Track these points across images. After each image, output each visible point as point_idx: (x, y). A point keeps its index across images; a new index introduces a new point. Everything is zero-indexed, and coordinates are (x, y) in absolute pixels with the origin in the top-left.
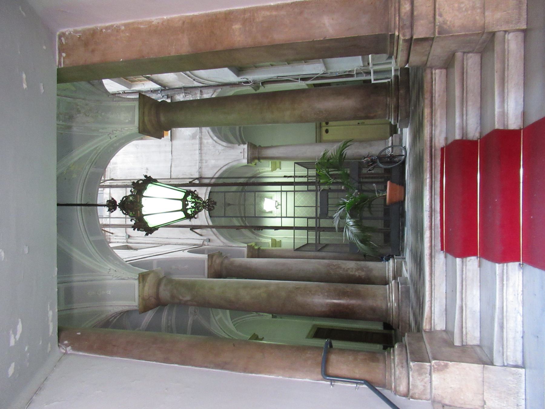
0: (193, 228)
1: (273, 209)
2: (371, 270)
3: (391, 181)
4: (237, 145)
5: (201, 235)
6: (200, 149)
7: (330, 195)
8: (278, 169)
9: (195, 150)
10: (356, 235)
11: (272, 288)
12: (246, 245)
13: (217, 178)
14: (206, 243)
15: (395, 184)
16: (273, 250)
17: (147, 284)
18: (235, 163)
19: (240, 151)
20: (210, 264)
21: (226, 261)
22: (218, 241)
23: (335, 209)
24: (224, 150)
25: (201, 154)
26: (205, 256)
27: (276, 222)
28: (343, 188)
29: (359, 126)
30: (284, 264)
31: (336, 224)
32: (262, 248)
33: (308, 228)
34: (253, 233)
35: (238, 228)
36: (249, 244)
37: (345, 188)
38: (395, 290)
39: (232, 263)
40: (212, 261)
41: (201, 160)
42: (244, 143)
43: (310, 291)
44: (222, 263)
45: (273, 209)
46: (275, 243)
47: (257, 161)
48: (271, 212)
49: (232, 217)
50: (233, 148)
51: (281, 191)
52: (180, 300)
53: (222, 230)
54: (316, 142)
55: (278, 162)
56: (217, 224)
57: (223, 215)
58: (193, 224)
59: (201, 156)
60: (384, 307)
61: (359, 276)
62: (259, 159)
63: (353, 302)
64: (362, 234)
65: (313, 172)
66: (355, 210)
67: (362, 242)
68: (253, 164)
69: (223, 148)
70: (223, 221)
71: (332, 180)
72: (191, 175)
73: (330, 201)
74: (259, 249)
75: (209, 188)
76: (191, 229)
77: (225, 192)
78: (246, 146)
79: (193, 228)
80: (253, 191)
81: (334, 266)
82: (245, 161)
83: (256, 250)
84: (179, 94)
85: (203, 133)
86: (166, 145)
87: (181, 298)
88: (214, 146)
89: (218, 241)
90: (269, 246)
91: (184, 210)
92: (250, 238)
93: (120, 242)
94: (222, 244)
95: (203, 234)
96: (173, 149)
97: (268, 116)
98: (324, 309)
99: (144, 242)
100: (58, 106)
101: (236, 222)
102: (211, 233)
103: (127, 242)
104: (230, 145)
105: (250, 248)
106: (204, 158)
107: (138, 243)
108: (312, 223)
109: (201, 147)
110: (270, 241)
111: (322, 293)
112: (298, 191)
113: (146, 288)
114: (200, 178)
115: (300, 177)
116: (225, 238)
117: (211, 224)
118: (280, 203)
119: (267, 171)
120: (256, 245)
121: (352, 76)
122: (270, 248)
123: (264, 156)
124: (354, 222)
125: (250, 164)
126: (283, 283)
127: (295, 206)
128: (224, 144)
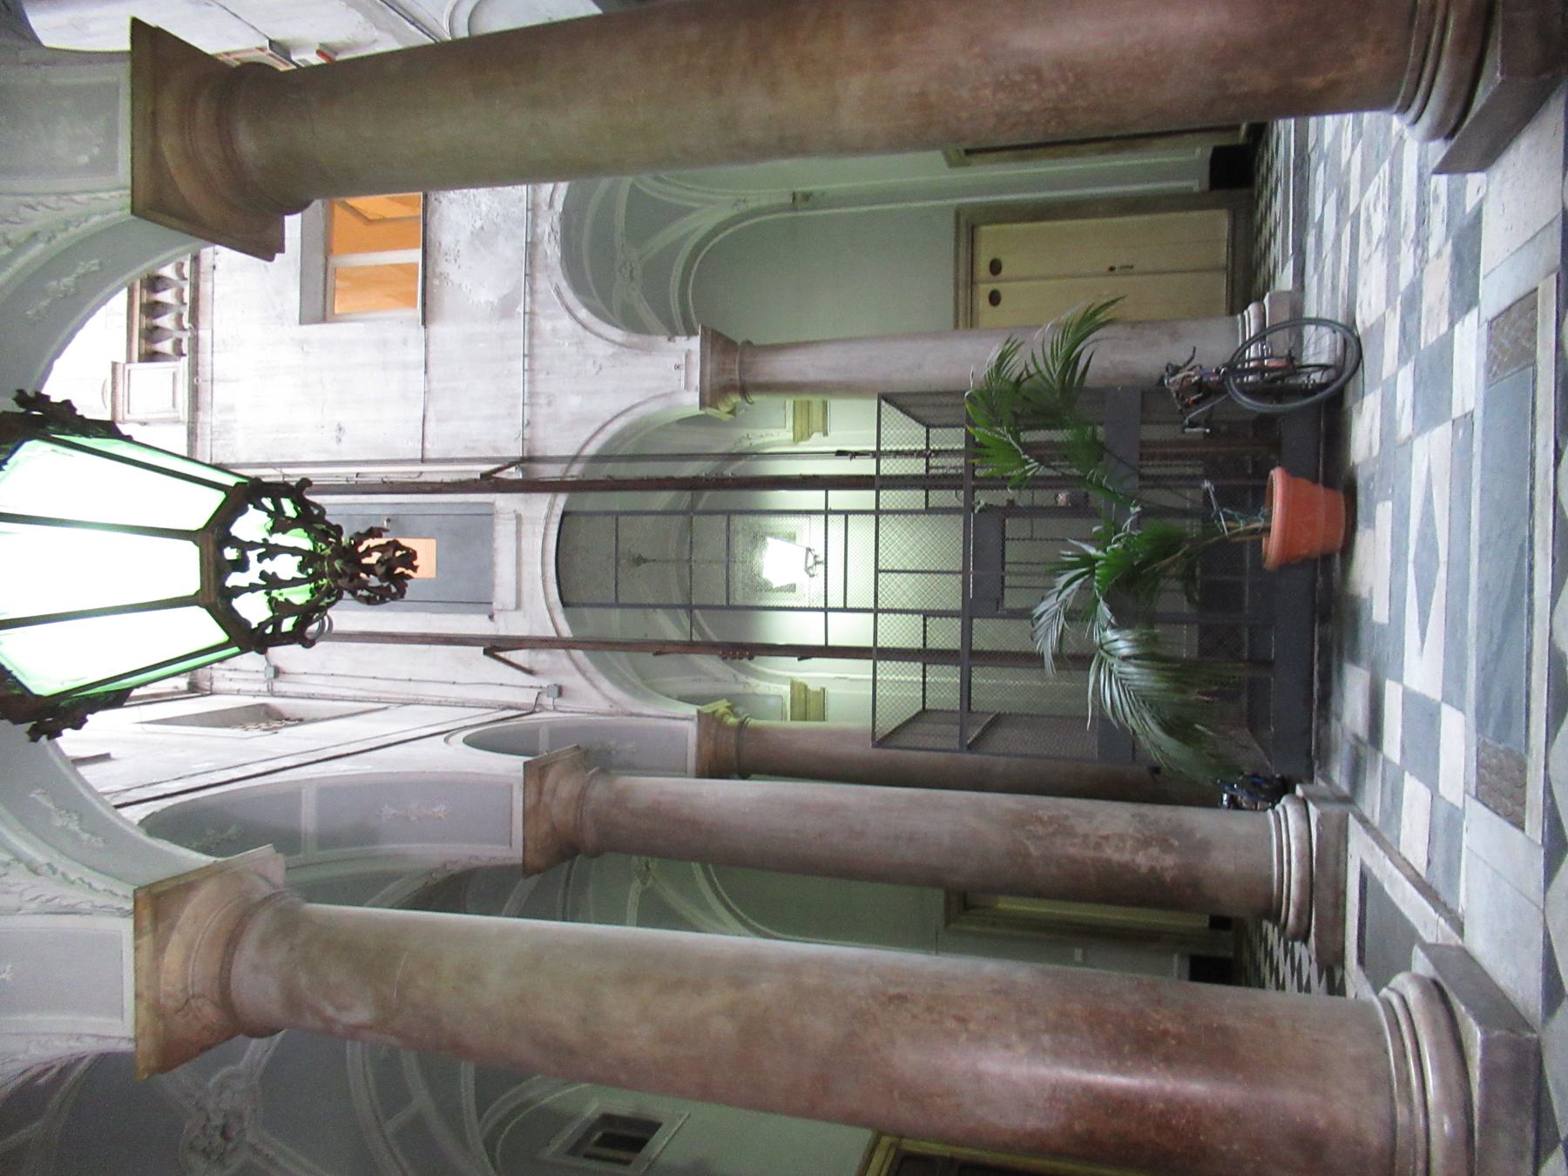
0: (495, 647)
1: (797, 575)
2: (1204, 846)
3: (1292, 472)
4: (662, 340)
5: (530, 672)
6: (529, 355)
7: (1013, 526)
8: (817, 436)
10: (1143, 699)
11: (765, 989)
12: (692, 710)
13: (597, 458)
14: (547, 701)
15: (1304, 482)
17: (175, 938)
18: (654, 408)
19: (674, 361)
20: (532, 799)
21: (599, 791)
22: (594, 694)
23: (1039, 582)
24: (613, 355)
25: (530, 370)
27: (807, 630)
29: (1112, 280)
30: (832, 809)
31: (1047, 645)
32: (752, 722)
33: (925, 656)
35: (661, 648)
36: (707, 709)
37: (1069, 499)
38: (1437, 1046)
39: (620, 800)
40: (540, 793)
41: (532, 395)
42: (690, 332)
43: (961, 1020)
44: (582, 796)
45: (797, 575)
46: (808, 703)
47: (736, 399)
48: (792, 588)
49: (650, 606)
50: (648, 350)
51: (827, 512)
52: (329, 1022)
53: (609, 655)
54: (956, 326)
55: (816, 401)
56: (590, 631)
57: (612, 599)
58: (502, 633)
59: (531, 382)
60: (1375, 1138)
61: (1152, 870)
62: (744, 390)
63: (1196, 1088)
64: (1177, 698)
65: (953, 439)
66: (1130, 591)
67: (1169, 728)
68: (724, 409)
69: (611, 350)
70: (616, 623)
71: (1033, 468)
72: (496, 449)
73: (1013, 552)
74: (742, 725)
75: (561, 500)
76: (486, 652)
77: (617, 515)
78: (695, 343)
79: (495, 647)
80: (722, 512)
82: (690, 401)
86: (405, 342)
87: (330, 1011)
88: (580, 344)
89: (590, 696)
90: (783, 717)
91: (215, 597)
92: (717, 680)
93: (247, 693)
94: (604, 706)
95: (536, 667)
96: (431, 356)
97: (756, 107)
98: (1032, 1122)
100: (1487, 806)
101: (669, 627)
102: (566, 663)
103: (272, 693)
104: (636, 339)
105: (708, 723)
106: (541, 387)
107: (310, 697)
108: (946, 635)
109: (531, 346)
110: (787, 689)
111: (1023, 1035)
112: (888, 512)
113: (173, 957)
114: (526, 460)
115: (898, 454)
116: (620, 682)
117: (566, 632)
118: (822, 558)
119: (774, 434)
120: (731, 709)
122: (789, 724)
123: (761, 379)
124: (1137, 642)
125: (710, 411)
126: (826, 963)
127: (877, 571)
128: (617, 334)
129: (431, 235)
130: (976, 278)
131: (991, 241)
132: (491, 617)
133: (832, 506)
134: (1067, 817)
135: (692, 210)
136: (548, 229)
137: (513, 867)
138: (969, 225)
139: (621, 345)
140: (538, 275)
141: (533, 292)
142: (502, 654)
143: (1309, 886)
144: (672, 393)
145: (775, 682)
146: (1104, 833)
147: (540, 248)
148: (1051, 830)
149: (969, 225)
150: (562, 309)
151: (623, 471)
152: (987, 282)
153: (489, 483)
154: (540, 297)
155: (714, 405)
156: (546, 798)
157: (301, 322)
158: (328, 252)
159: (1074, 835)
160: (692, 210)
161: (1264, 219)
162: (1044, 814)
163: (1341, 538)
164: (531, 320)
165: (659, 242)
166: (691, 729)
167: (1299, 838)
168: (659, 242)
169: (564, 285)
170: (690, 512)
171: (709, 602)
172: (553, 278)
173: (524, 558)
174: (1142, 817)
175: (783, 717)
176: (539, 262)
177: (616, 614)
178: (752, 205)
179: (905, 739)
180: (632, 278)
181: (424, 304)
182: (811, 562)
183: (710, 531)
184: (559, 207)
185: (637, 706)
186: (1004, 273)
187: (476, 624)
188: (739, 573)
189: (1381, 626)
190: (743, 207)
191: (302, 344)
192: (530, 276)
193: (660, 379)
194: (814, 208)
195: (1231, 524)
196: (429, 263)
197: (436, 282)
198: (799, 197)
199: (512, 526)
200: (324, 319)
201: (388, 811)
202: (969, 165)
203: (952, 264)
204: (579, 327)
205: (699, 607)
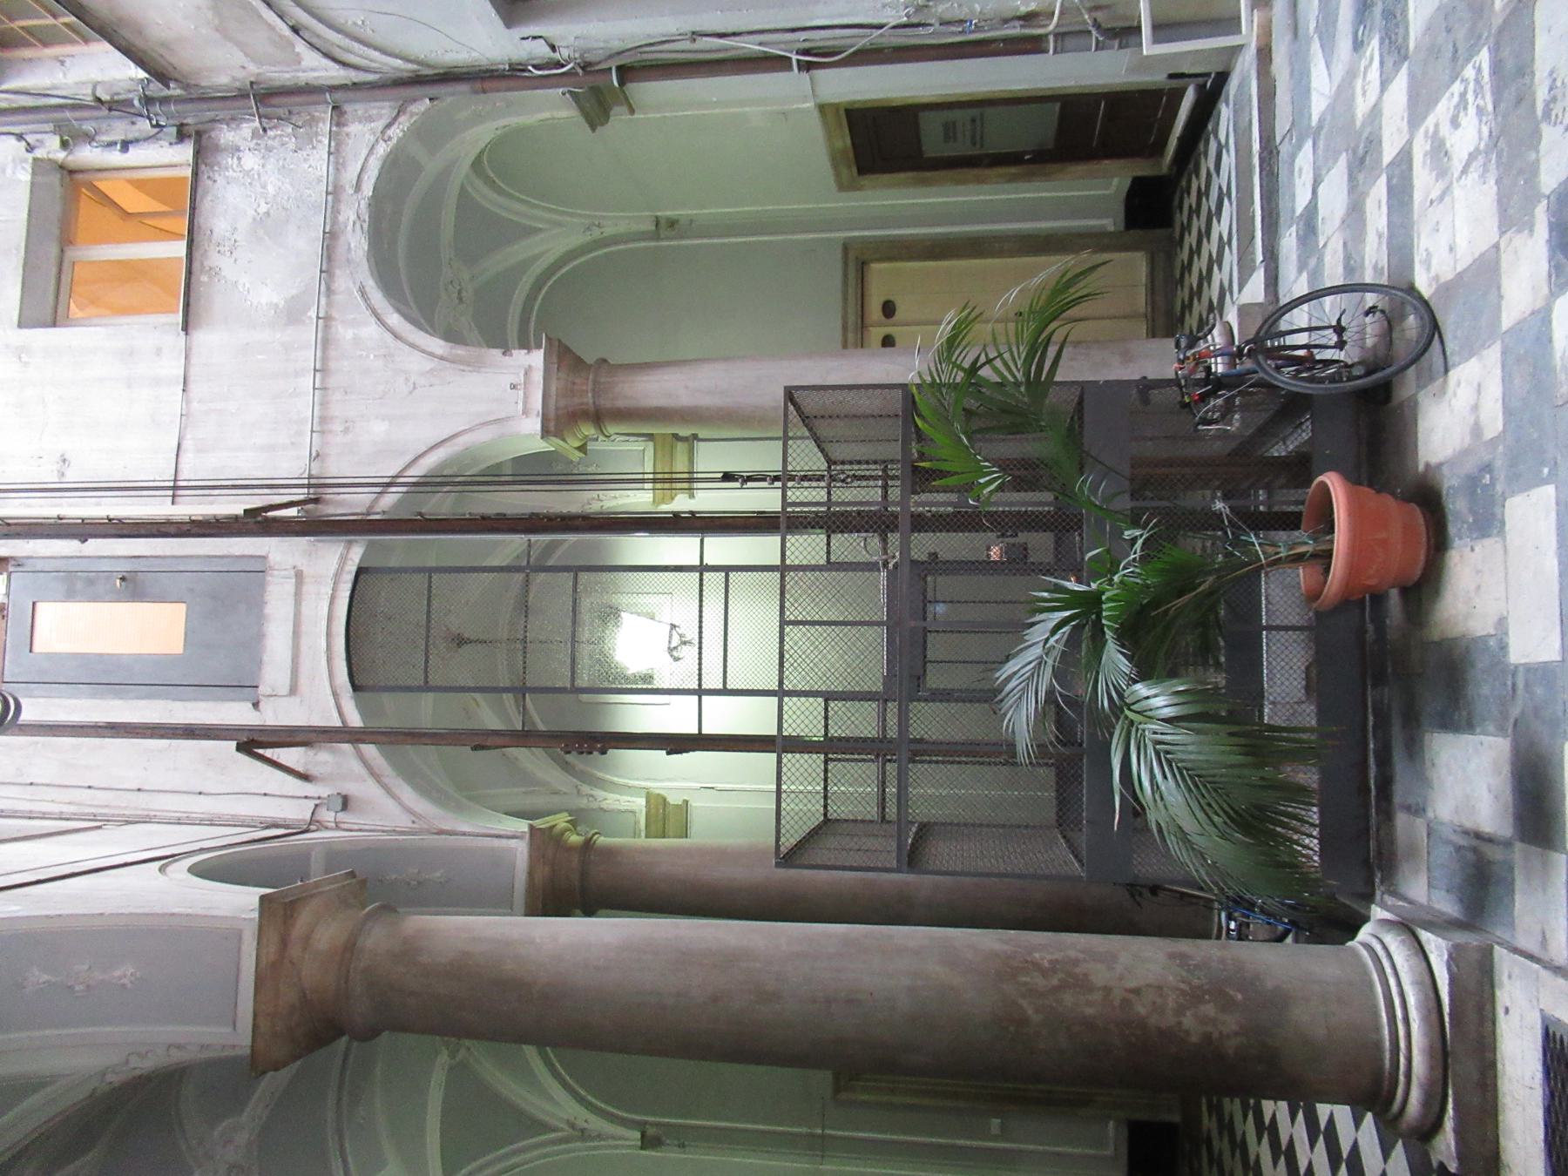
0: (252, 743)
2: (1279, 1001)
5: (305, 777)
6: (322, 370)
7: (942, 584)
9: (297, 374)
12: (523, 826)
16: (655, 851)
18: (483, 436)
20: (272, 950)
21: (377, 939)
22: (390, 804)
26: (242, 901)
27: (677, 717)
28: (995, 553)
30: (730, 959)
32: (601, 840)
33: (831, 748)
34: (567, 767)
35: (482, 741)
36: (539, 823)
37: (1007, 550)
39: (408, 952)
40: (284, 942)
44: (350, 948)
46: (666, 816)
47: (588, 430)
50: (476, 365)
53: (412, 751)
56: (391, 722)
59: (324, 404)
61: (1207, 1037)
62: (599, 417)
64: (1254, 776)
69: (429, 364)
70: (426, 711)
74: (588, 845)
76: (239, 749)
78: (537, 358)
79: (252, 743)
81: (1044, 973)
83: (570, 849)
84: (233, 120)
85: (338, 298)
89: (384, 807)
94: (404, 822)
95: (314, 771)
96: (193, 371)
99: (25, 806)
101: (489, 717)
102: (356, 766)
104: (460, 351)
105: (543, 842)
106: (336, 410)
108: (858, 721)
109: (325, 359)
110: (642, 801)
116: (426, 789)
117: (355, 720)
118: (692, 634)
121: (1033, 45)
122: (642, 841)
123: (621, 404)
127: (783, 623)
128: (437, 345)
129: (200, 220)
130: (868, 321)
131: (883, 279)
132: (256, 705)
133: (710, 560)
134: (1076, 962)
135: (537, 230)
136: (353, 217)
137: (235, 1060)
138: (859, 261)
139: (441, 358)
140: (338, 272)
141: (330, 292)
142: (268, 753)
143: (1442, 1055)
144: (508, 418)
145: (642, 778)
146: (1132, 984)
147: (342, 240)
148: (1055, 982)
149: (859, 261)
150: (368, 313)
151: (440, 505)
152: (880, 326)
153: (257, 523)
154: (339, 298)
155: (559, 434)
156: (295, 951)
157: (20, 325)
158: (66, 240)
159: (1091, 989)
160: (537, 230)
161: (1196, 251)
162: (1043, 958)
163: (1421, 564)
164: (327, 327)
165: (494, 264)
166: (521, 849)
167: (1417, 983)
168: (494, 264)
169: (370, 284)
170: (530, 568)
171: (549, 684)
172: (356, 273)
173: (304, 628)
174: (1183, 957)
175: (635, 834)
176: (340, 251)
177: (427, 700)
178: (609, 230)
179: (820, 854)
180: (460, 299)
181: (187, 305)
182: (676, 641)
183: (551, 591)
184: (368, 189)
185: (449, 821)
186: (900, 315)
187: (237, 713)
188: (584, 651)
189: (1542, 673)
190: (596, 233)
191: (20, 352)
192: (327, 272)
193: (496, 401)
194: (682, 238)
195: (1270, 550)
196: (197, 255)
197: (204, 278)
198: (663, 222)
199: (290, 586)
200: (54, 324)
201: (38, 977)
202: (861, 188)
203: (839, 296)
204: (388, 337)
205: (534, 690)
